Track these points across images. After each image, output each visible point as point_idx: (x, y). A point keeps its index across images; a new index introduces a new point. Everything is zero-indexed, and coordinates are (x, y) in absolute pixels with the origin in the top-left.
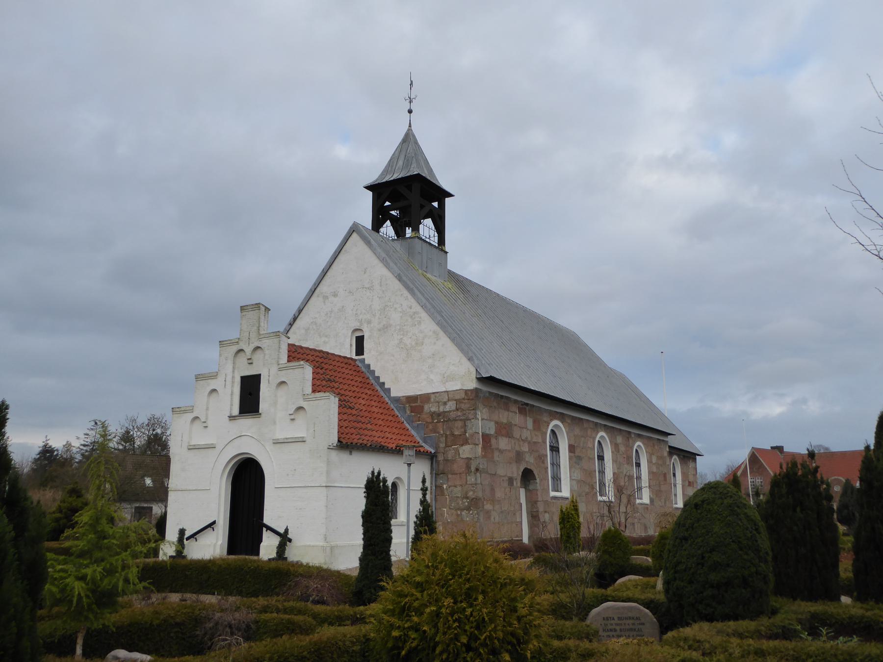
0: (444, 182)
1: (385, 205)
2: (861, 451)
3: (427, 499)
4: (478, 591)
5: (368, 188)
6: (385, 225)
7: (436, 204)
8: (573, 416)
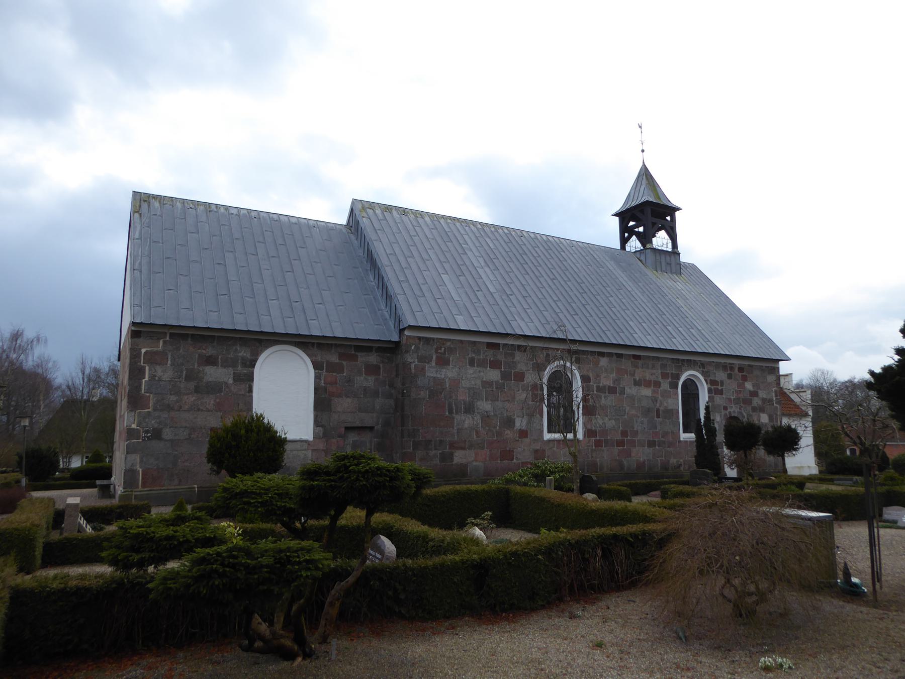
0: (674, 201)
1: (629, 225)
2: (327, 228)
3: (546, 409)
4: (626, 490)
5: (616, 215)
6: (631, 240)
7: (668, 218)
8: (426, 338)
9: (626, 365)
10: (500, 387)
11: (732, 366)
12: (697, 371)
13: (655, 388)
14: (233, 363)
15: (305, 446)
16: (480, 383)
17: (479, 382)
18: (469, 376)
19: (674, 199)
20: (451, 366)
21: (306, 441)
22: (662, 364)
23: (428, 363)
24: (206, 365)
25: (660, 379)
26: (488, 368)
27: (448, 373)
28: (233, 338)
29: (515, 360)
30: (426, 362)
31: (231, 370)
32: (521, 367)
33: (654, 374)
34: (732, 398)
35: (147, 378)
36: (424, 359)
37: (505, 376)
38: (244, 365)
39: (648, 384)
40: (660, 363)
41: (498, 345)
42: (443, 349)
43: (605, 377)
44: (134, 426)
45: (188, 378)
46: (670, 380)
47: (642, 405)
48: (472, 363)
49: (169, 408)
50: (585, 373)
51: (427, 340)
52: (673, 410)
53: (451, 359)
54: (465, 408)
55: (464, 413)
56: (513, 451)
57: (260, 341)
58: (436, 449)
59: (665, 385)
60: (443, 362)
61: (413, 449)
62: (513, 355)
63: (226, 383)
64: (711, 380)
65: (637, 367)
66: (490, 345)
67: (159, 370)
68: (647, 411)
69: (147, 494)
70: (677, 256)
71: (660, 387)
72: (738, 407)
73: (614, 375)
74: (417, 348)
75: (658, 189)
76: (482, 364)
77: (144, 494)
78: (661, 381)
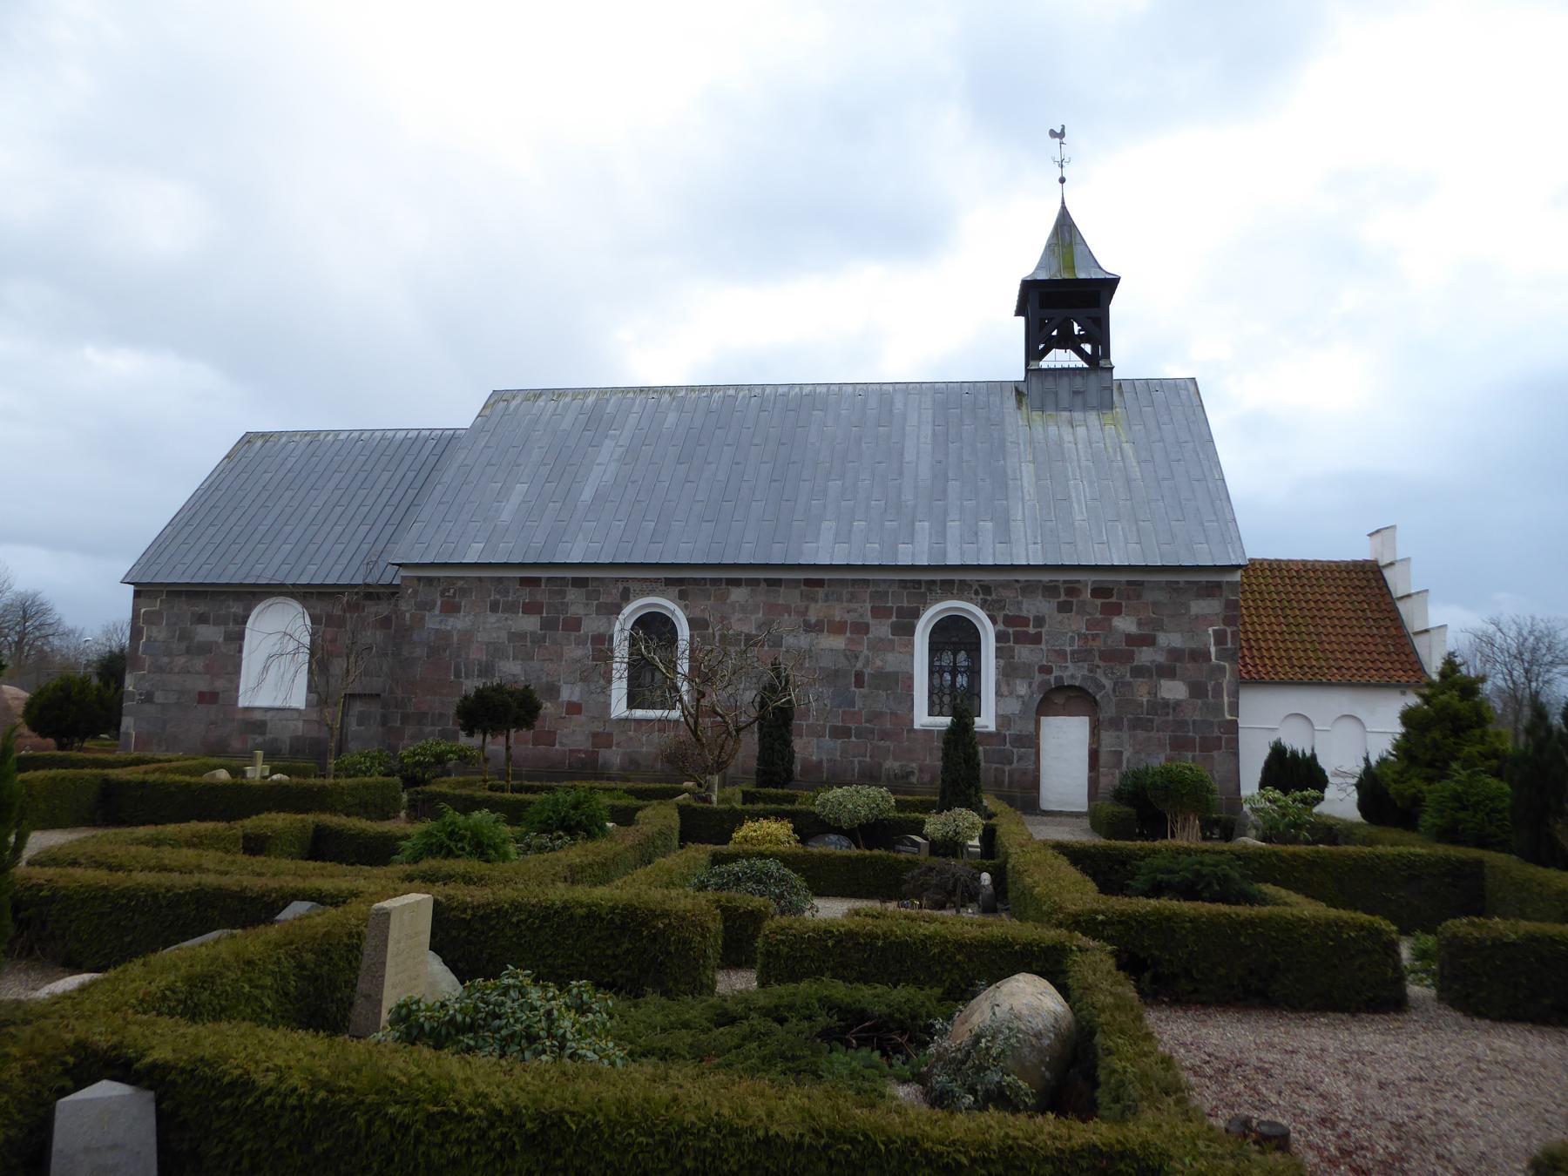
9: (792, 597)
10: (538, 641)
11: (1076, 585)
12: (970, 600)
13: (855, 636)
14: (220, 621)
15: (296, 715)
16: (506, 636)
17: (504, 635)
18: (488, 626)
19: (1109, 261)
20: (462, 613)
21: (297, 710)
22: (876, 592)
23: (429, 611)
24: (199, 623)
25: (869, 619)
26: (520, 614)
27: (458, 623)
28: (225, 592)
29: (566, 600)
30: (425, 610)
31: (222, 628)
32: (576, 610)
33: (855, 610)
34: (1068, 649)
35: (144, 640)
36: (427, 606)
37: (548, 625)
38: (236, 622)
39: (838, 628)
40: (869, 591)
41: (539, 579)
42: (452, 591)
43: (739, 620)
45: (181, 638)
46: (894, 619)
47: (821, 665)
48: (494, 608)
49: (160, 670)
50: (697, 613)
51: (430, 581)
52: (897, 673)
53: (463, 604)
54: (480, 671)
55: (478, 676)
56: (555, 733)
57: (253, 594)
58: (433, 725)
59: (881, 629)
60: (451, 608)
61: (402, 723)
62: (563, 594)
63: (216, 642)
64: (1006, 617)
65: (814, 600)
66: (525, 581)
67: (155, 630)
68: (833, 676)
70: (1105, 375)
71: (867, 633)
72: (1086, 666)
73: (761, 615)
74: (415, 592)
75: (1078, 249)
76: (511, 608)
78: (871, 621)
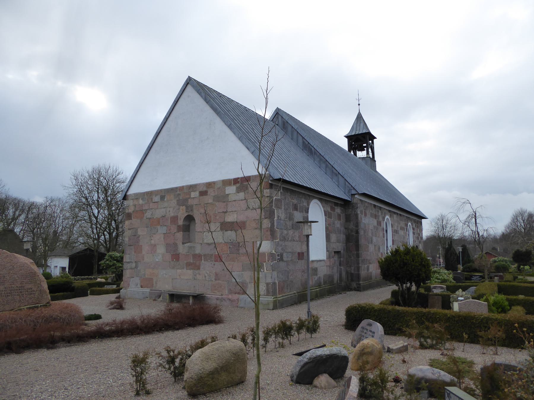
5: (346, 137)
7: (370, 142)
21: (323, 260)
44: (274, 252)
69: (283, 299)
77: (528, 287)
